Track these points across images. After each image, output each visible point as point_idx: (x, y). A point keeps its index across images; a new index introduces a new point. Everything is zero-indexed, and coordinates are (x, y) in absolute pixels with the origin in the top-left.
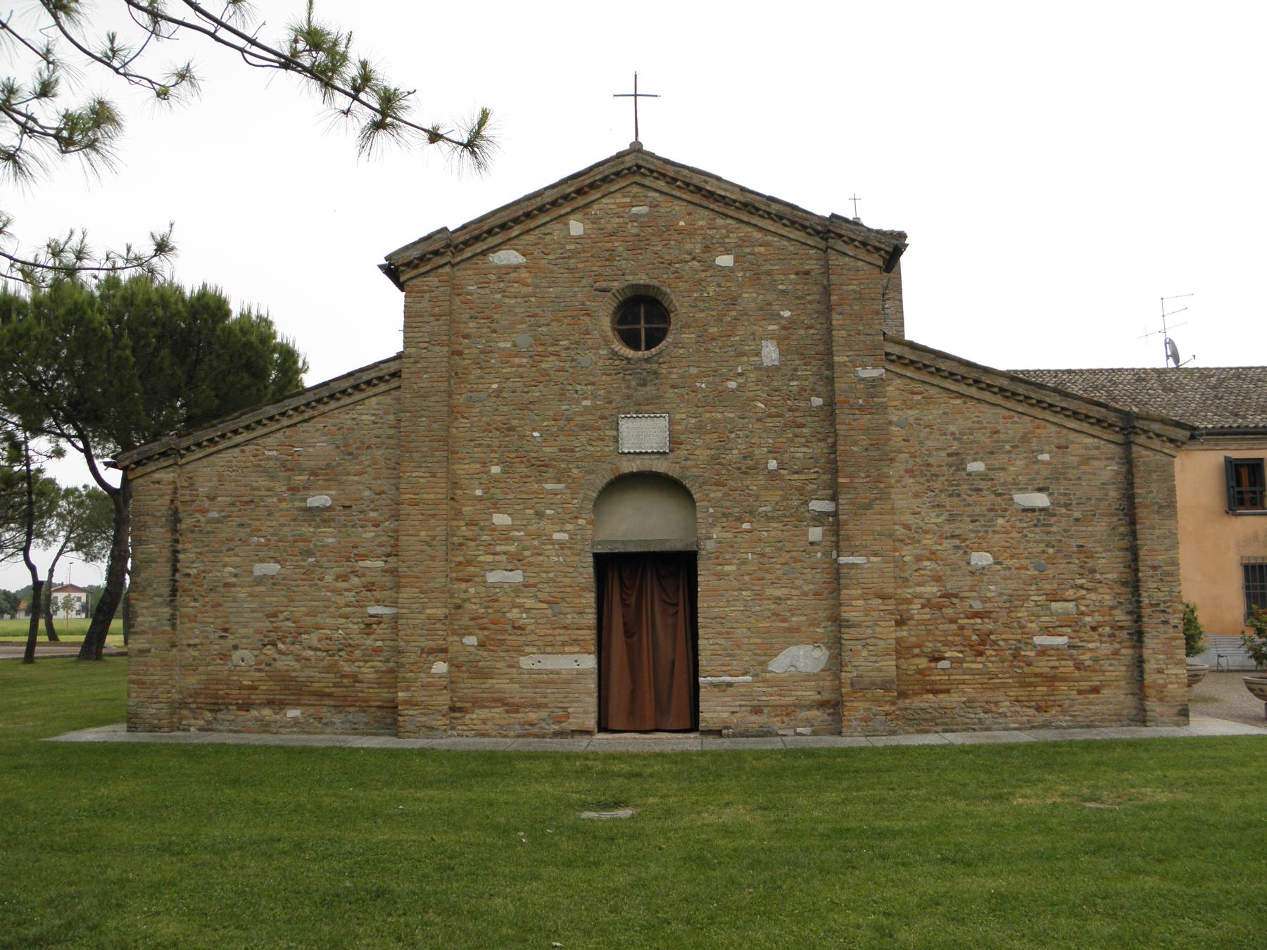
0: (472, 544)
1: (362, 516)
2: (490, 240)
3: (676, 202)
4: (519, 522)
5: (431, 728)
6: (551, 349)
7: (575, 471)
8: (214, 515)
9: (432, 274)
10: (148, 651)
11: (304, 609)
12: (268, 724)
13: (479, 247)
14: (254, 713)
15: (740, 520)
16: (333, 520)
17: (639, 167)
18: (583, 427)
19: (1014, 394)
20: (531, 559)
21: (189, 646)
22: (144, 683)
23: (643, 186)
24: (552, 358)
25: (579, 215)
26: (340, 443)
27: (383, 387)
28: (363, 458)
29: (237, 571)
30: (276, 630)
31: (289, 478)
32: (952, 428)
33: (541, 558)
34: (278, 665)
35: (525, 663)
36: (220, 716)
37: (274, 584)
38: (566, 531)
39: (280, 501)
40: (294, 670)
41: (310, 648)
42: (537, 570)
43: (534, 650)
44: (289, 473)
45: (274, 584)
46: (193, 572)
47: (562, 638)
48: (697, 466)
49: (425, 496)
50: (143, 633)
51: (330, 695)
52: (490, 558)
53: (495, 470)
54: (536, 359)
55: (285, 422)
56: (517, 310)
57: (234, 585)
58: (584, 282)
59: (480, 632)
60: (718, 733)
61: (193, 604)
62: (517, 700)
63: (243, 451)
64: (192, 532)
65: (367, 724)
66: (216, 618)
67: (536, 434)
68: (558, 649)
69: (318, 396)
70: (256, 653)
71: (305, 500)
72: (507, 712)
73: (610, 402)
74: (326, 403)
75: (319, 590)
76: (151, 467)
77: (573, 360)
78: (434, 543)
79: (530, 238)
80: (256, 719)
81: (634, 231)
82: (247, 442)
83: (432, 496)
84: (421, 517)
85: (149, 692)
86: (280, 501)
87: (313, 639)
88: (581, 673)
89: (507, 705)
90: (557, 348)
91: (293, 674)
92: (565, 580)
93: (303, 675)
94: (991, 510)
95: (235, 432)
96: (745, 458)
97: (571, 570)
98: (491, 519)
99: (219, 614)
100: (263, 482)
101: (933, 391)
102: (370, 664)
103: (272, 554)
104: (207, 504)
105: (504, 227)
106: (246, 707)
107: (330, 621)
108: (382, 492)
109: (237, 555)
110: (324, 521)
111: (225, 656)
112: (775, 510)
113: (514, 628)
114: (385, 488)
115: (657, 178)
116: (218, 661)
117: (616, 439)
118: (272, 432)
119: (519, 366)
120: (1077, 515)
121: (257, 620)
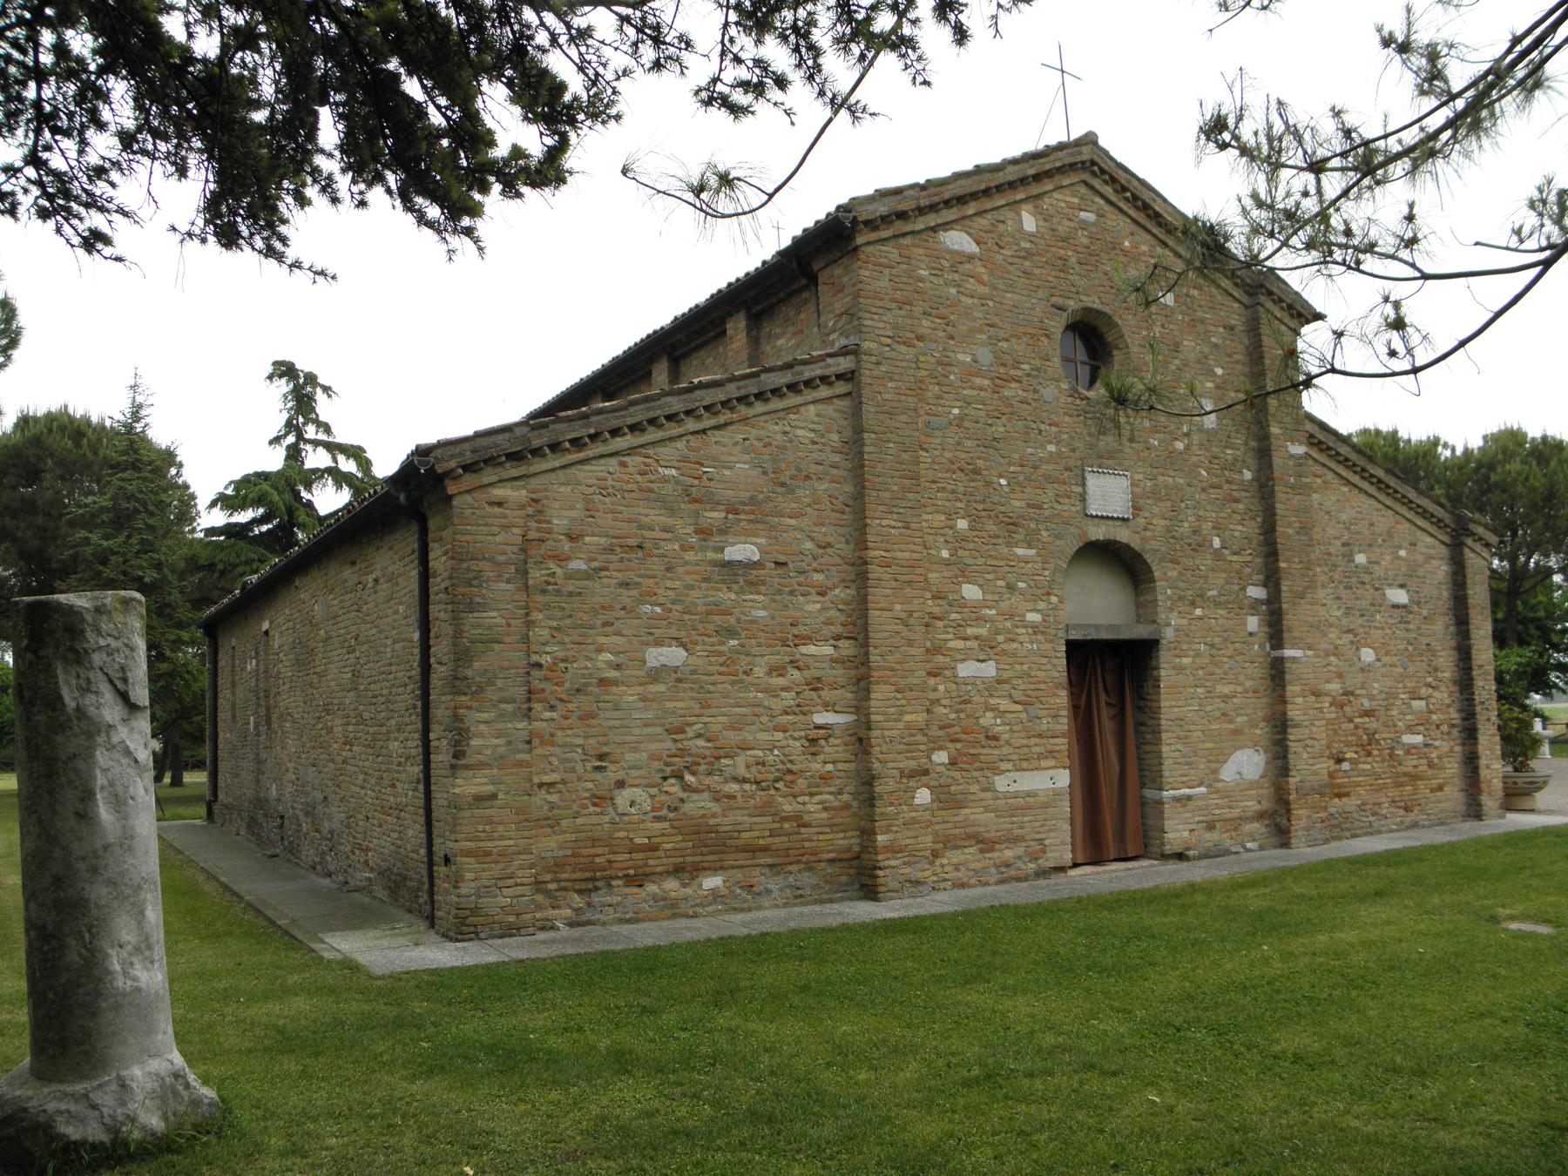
0: (940, 624)
1: (801, 579)
2: (944, 212)
3: (1121, 216)
4: (989, 597)
5: (917, 883)
6: (1013, 372)
7: (1044, 533)
8: (578, 565)
9: (891, 243)
10: (494, 796)
11: (724, 719)
12: (674, 904)
13: (932, 219)
14: (652, 888)
15: (1193, 604)
16: (763, 582)
17: (1093, 163)
18: (1048, 478)
19: (1388, 486)
20: (1004, 646)
21: (541, 785)
22: (488, 854)
23: (1092, 188)
24: (1014, 385)
25: (1030, 206)
26: (768, 466)
27: (824, 392)
28: (799, 492)
29: (620, 659)
30: (682, 753)
31: (697, 514)
32: (1344, 517)
33: (1015, 645)
34: (687, 808)
35: (1001, 783)
36: (596, 898)
37: (679, 680)
38: (1038, 611)
39: (684, 548)
40: (714, 815)
41: (735, 779)
42: (1010, 660)
43: (1009, 766)
44: (697, 506)
45: (679, 680)
46: (546, 660)
47: (1036, 749)
48: (1154, 538)
49: (899, 555)
50: (482, 765)
51: (766, 849)
52: (960, 644)
53: (962, 524)
54: (999, 382)
55: (691, 425)
56: (975, 314)
57: (615, 683)
58: (1041, 293)
59: (951, 745)
60: (1180, 856)
61: (547, 715)
62: (993, 834)
63: (623, 464)
64: (544, 592)
65: (815, 887)
66: (587, 737)
67: (1003, 482)
68: (1035, 763)
69: (743, 392)
70: (654, 791)
71: (722, 550)
72: (982, 851)
73: (1073, 450)
74: (750, 405)
75: (746, 689)
76: (489, 475)
77: (1035, 391)
78: (911, 621)
79: (984, 222)
80: (655, 898)
81: (1085, 241)
82: (631, 451)
83: (907, 555)
84: (894, 584)
85: (497, 870)
86: (684, 548)
87: (740, 765)
88: (1057, 793)
89: (982, 842)
90: (1019, 373)
91: (712, 822)
92: (1039, 673)
93: (725, 822)
94: (1373, 605)
95: (615, 432)
96: (1195, 532)
97: (1045, 661)
98: (959, 591)
99: (592, 731)
100: (656, 517)
101: (1330, 476)
102: (818, 798)
103: (673, 632)
104: (567, 546)
105: (961, 200)
106: (637, 880)
107: (761, 736)
108: (829, 545)
109: (618, 633)
110: (751, 583)
111: (600, 800)
112: (1221, 595)
113: (987, 737)
114: (831, 539)
115: (1106, 182)
116: (592, 809)
117: (1083, 498)
118: (671, 439)
119: (981, 389)
120: (1425, 612)
121: (653, 738)
